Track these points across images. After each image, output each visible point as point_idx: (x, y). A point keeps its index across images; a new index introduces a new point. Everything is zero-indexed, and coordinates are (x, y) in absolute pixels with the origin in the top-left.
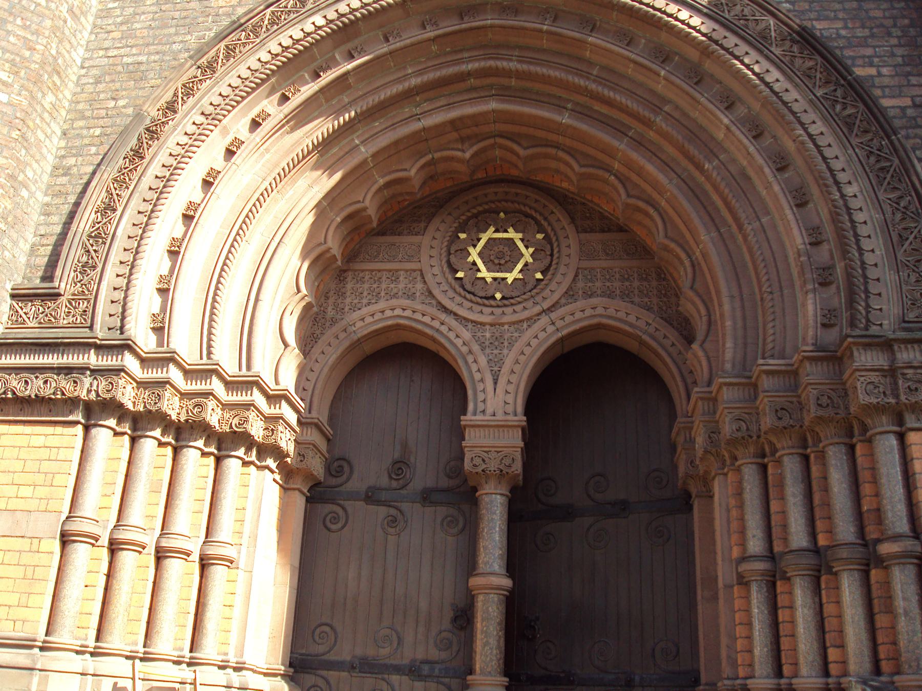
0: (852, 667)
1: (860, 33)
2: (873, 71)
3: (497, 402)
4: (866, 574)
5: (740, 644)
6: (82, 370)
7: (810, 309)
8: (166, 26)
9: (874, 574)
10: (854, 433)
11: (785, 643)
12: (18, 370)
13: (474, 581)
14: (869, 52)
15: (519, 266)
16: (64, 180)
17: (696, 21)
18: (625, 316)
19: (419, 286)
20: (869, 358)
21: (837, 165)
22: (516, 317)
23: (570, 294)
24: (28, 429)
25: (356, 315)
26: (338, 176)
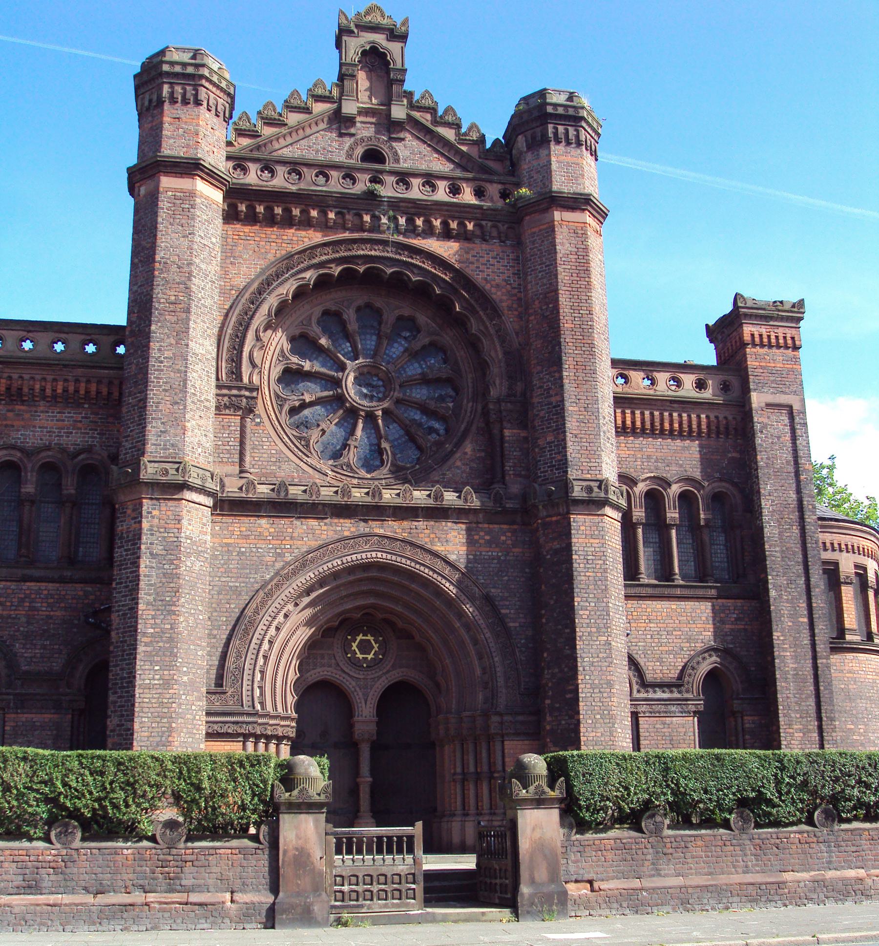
0: (485, 807)
1: (506, 594)
2: (508, 611)
3: (366, 711)
4: (490, 781)
5: (453, 801)
6: (243, 723)
7: (480, 697)
8: (245, 568)
9: (492, 781)
10: (490, 739)
11: (466, 800)
12: (217, 723)
13: (358, 780)
14: (507, 603)
15: (373, 652)
16: (214, 640)
17: (451, 588)
18: (413, 675)
19: (333, 661)
20: (495, 719)
21: (493, 650)
22: (372, 676)
23: (394, 667)
24: (223, 743)
25: (309, 674)
26: (313, 629)
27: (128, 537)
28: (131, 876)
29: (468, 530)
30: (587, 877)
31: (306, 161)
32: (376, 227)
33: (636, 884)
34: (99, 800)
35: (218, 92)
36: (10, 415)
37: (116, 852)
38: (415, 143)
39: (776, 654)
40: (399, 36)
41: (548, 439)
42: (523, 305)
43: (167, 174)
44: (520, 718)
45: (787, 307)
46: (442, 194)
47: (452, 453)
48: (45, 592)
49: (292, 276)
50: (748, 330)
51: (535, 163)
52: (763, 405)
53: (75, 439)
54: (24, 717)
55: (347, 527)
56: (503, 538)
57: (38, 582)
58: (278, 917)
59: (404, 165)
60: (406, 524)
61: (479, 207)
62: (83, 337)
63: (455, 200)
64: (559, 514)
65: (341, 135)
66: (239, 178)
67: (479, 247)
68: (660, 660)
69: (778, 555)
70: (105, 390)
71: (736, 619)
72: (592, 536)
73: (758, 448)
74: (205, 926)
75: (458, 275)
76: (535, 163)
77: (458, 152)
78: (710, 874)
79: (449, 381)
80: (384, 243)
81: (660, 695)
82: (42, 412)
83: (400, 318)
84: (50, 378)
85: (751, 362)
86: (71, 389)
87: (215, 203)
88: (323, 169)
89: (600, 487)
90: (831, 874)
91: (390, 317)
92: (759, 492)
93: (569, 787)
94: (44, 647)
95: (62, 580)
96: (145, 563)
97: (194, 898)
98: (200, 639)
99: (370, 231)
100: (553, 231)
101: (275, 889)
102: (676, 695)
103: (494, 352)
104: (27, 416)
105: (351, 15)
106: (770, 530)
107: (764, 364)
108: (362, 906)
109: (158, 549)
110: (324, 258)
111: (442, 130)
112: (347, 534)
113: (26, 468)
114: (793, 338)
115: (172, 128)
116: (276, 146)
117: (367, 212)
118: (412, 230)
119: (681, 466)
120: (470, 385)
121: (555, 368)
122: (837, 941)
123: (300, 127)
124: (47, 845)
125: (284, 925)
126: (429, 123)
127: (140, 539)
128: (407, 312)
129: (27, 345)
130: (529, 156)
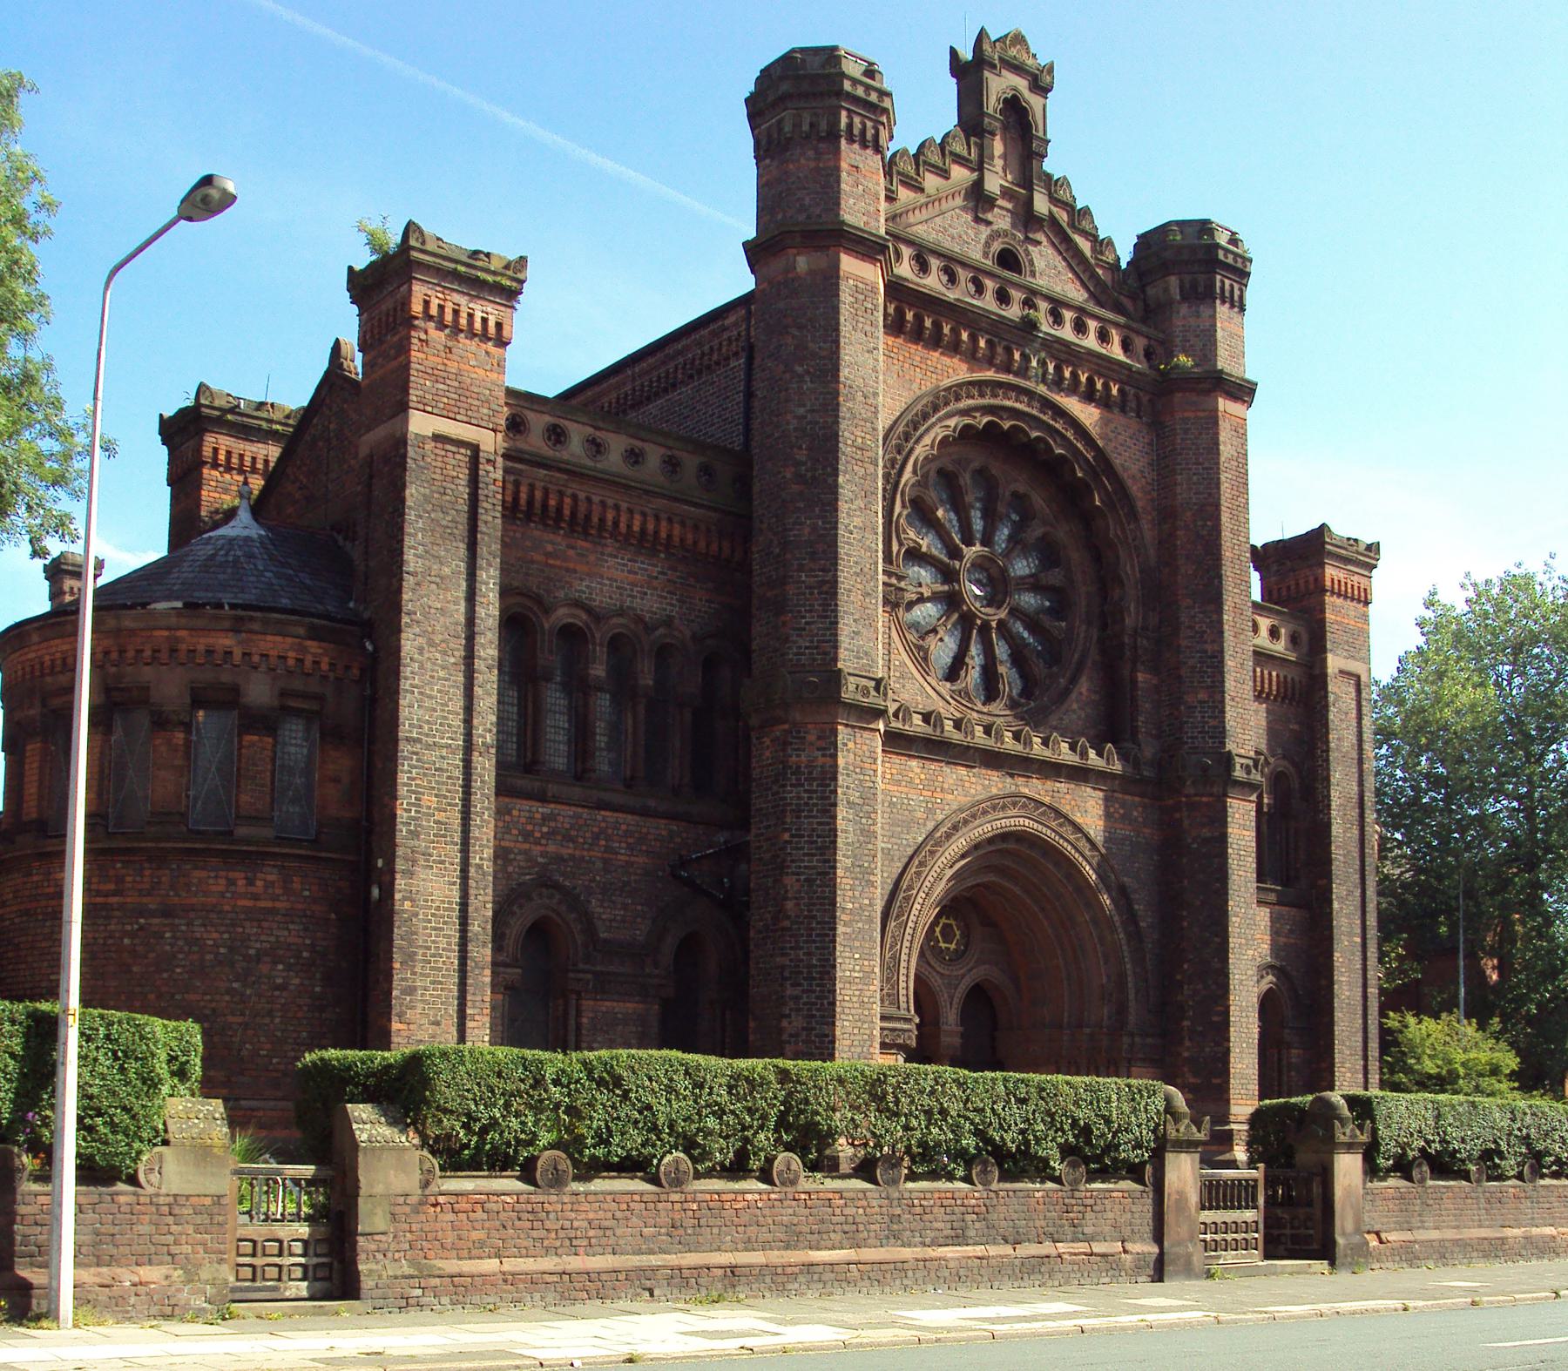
27: (810, 773)
28: (1043, 1223)
29: (1106, 799)
30: (1376, 1228)
31: (965, 260)
32: (1023, 372)
33: (1408, 1236)
34: (1022, 1132)
36: (571, 552)
37: (1029, 1194)
38: (1050, 251)
40: (1041, 86)
41: (1200, 696)
42: (1167, 514)
43: (849, 251)
44: (1149, 1040)
45: (495, 265)
48: (624, 827)
49: (940, 420)
50: (421, 293)
51: (1192, 321)
53: (651, 604)
55: (995, 783)
57: (616, 811)
58: (1168, 1269)
59: (1041, 282)
60: (1049, 784)
61: (1128, 368)
64: (1211, 795)
65: (977, 220)
67: (1118, 419)
71: (1291, 931)
73: (1331, 726)
74: (1107, 1280)
75: (1100, 453)
76: (1192, 321)
77: (1094, 276)
78: (1457, 1227)
80: (1030, 394)
82: (610, 555)
85: (1330, 616)
86: (651, 527)
88: (952, 266)
89: (877, 689)
90: (1535, 1231)
92: (1327, 779)
93: (1374, 1131)
94: (625, 907)
95: (645, 813)
96: (842, 813)
97: (1098, 1248)
99: (1016, 374)
100: (1216, 423)
101: (1158, 1237)
103: (1130, 570)
104: (592, 558)
106: (1337, 829)
108: (1218, 1257)
109: (855, 796)
111: (1078, 239)
113: (593, 636)
114: (499, 326)
115: (850, 180)
116: (912, 220)
117: (1020, 346)
118: (1058, 383)
121: (1211, 607)
122: (517, 1367)
124: (532, 1188)
125: (1171, 1279)
126: (1069, 228)
127: (835, 779)
128: (1021, 488)
130: (1184, 309)
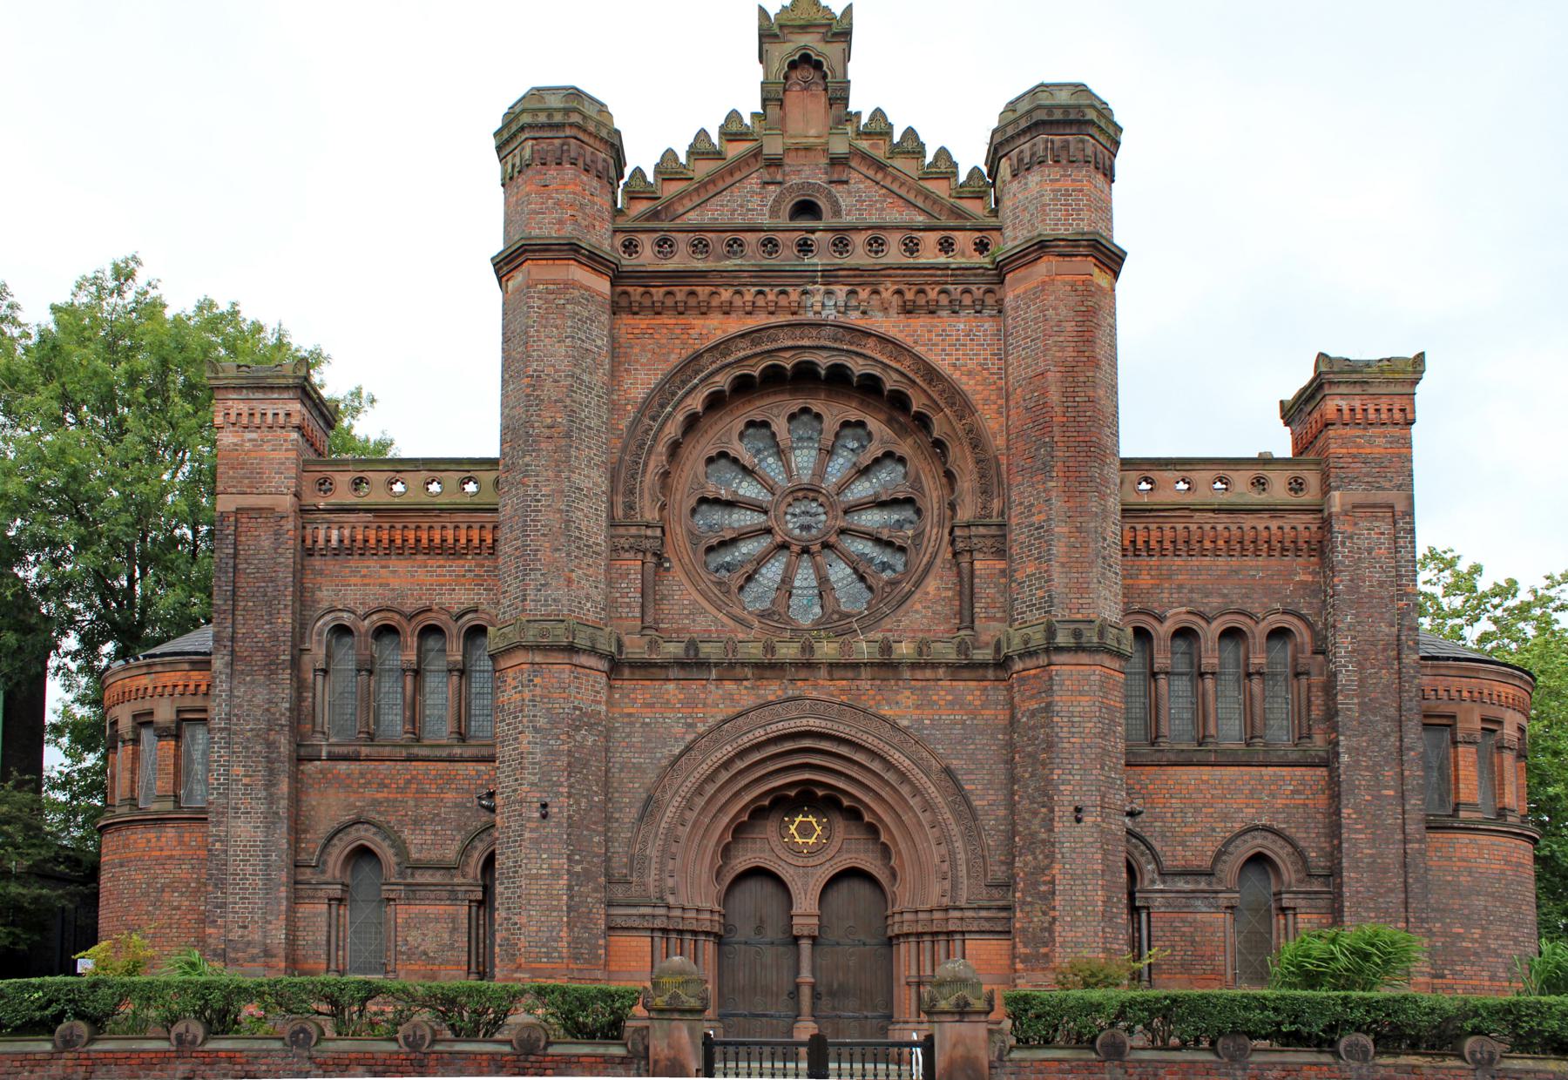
35: (597, 144)
39: (1345, 836)
41: (1028, 571)
46: (894, 254)
47: (910, 594)
52: (1349, 507)
54: (415, 910)
55: (744, 694)
56: (970, 698)
62: (424, 475)
63: (634, 262)
66: (628, 262)
68: (1183, 844)
69: (1356, 708)
70: (385, 537)
72: (1081, 693)
79: (909, 501)
81: (1181, 885)
83: (846, 424)
84: (425, 526)
87: (600, 294)
91: (831, 423)
94: (435, 833)
98: (595, 823)
102: (1203, 886)
105: (773, 11)
107: (1354, 451)
110: (741, 354)
112: (771, 698)
119: (1225, 596)
120: (936, 506)
123: (712, 180)
128: (854, 415)
129: (435, 488)
